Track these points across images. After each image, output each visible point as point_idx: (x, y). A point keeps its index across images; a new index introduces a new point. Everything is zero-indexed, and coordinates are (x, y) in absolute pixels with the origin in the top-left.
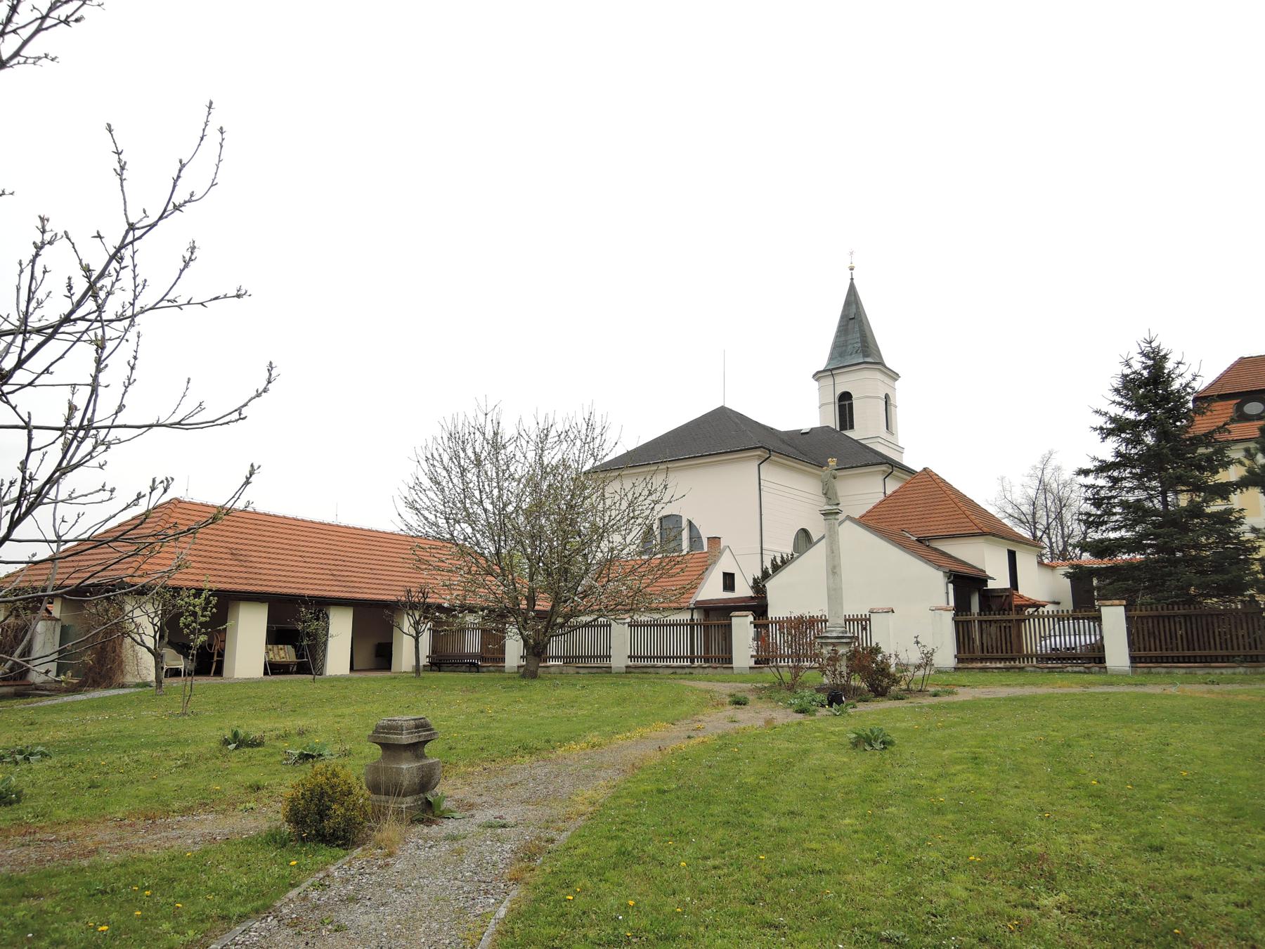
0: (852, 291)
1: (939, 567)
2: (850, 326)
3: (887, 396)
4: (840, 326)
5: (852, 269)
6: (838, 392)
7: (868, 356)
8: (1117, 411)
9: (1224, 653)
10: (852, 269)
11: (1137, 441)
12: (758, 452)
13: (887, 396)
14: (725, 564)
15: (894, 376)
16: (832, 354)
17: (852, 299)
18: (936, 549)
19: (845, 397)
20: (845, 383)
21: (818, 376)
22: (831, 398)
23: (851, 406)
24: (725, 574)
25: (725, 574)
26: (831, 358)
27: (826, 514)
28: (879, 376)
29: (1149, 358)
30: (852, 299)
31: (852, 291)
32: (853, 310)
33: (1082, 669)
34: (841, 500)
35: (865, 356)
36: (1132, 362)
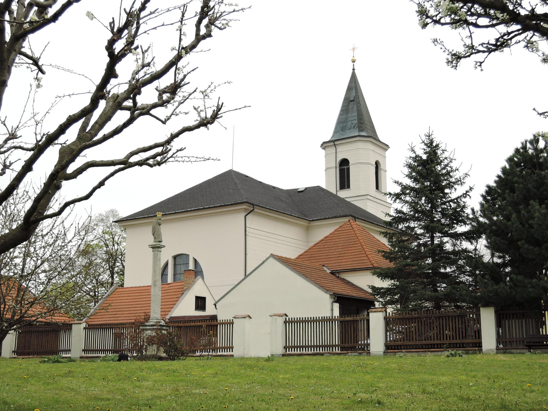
0: (354, 79)
1: (326, 290)
2: (350, 106)
3: (377, 164)
4: (343, 107)
5: (354, 61)
6: (339, 159)
7: (362, 131)
8: (408, 182)
9: (438, 342)
10: (354, 61)
11: (504, 199)
12: (244, 206)
13: (377, 164)
14: (199, 288)
15: (386, 147)
16: (336, 128)
17: (354, 85)
18: (343, 280)
19: (344, 163)
20: (345, 151)
21: (324, 145)
22: (334, 164)
23: (348, 169)
24: (197, 298)
25: (197, 298)
26: (336, 132)
27: (154, 247)
28: (370, 146)
29: (429, 147)
30: (354, 85)
31: (354, 79)
32: (353, 94)
33: (356, 354)
34: (163, 239)
35: (361, 130)
36: (416, 149)
